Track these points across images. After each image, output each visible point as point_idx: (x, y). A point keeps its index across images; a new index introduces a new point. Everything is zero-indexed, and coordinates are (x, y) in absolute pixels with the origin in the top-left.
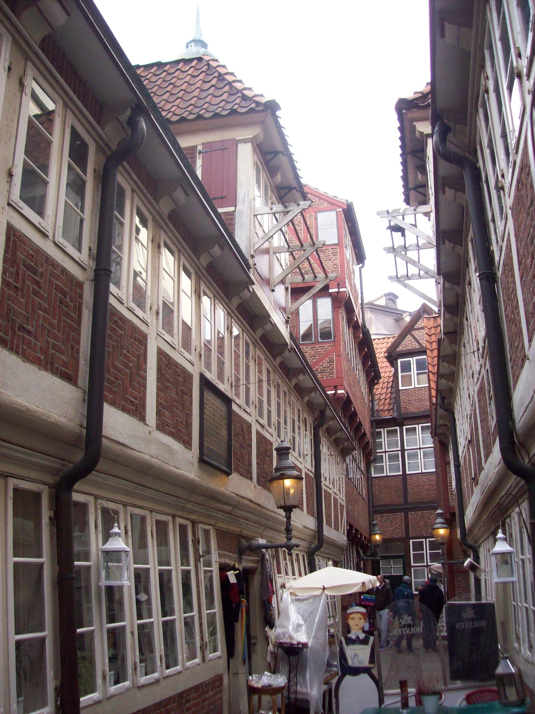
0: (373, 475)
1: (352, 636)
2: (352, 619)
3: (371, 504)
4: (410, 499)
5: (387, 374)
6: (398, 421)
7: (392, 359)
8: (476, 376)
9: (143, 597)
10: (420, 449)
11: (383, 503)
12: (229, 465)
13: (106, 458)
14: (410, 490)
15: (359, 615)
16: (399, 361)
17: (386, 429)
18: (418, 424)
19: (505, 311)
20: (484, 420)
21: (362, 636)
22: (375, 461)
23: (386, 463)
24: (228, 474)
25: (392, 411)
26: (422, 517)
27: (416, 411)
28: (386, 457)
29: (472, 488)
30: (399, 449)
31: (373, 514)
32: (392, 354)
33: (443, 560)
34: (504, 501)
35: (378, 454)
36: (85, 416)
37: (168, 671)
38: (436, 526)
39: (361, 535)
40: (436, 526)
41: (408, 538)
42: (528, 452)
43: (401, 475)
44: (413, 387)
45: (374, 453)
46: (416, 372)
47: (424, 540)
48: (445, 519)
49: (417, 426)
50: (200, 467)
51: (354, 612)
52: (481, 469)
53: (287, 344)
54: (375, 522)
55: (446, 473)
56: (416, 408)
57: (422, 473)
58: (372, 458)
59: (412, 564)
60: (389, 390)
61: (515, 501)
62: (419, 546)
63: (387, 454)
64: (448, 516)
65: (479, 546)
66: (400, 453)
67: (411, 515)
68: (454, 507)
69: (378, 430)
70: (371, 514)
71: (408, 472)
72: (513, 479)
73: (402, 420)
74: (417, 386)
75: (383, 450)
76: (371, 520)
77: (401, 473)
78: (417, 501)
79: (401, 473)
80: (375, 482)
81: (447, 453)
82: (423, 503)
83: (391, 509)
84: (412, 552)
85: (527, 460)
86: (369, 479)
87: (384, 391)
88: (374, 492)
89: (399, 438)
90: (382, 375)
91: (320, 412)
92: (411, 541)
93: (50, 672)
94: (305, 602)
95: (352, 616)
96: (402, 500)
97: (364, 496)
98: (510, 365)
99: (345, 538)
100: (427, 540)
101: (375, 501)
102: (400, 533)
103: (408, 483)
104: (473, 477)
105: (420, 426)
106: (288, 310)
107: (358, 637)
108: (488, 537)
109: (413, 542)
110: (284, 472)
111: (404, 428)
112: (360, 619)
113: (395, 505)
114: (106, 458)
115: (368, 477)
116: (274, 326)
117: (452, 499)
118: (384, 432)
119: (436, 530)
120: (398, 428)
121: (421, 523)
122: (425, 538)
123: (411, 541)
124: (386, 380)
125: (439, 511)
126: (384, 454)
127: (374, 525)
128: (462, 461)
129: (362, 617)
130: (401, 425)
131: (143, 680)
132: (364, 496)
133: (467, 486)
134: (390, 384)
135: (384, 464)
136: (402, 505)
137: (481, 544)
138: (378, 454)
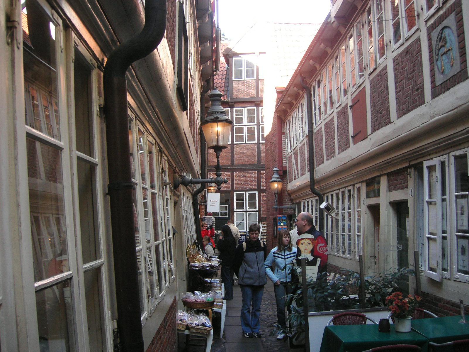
2: (302, 244)
4: (236, 162)
6: (230, 104)
7: (228, 57)
9: (349, 223)
10: (245, 125)
14: (236, 156)
15: (308, 241)
16: (234, 59)
18: (245, 107)
21: (311, 258)
25: (226, 96)
26: (244, 176)
32: (229, 53)
36: (444, 80)
38: (272, 180)
40: (272, 180)
41: (233, 190)
43: (230, 144)
46: (243, 69)
47: (245, 192)
49: (243, 108)
51: (304, 238)
56: (244, 95)
57: (245, 144)
59: (235, 210)
62: (240, 198)
63: (246, 127)
67: (236, 174)
68: (286, 167)
71: (235, 143)
73: (233, 103)
74: (246, 79)
75: (244, 124)
77: (256, 142)
78: (241, 164)
79: (256, 142)
87: (220, 81)
88: (209, 156)
92: (235, 193)
93: (108, 311)
96: (230, 162)
100: (247, 192)
103: (235, 150)
105: (246, 108)
109: (236, 194)
111: (234, 109)
112: (309, 244)
117: (285, 161)
119: (272, 184)
120: (229, 109)
121: (244, 180)
122: (246, 191)
123: (235, 193)
126: (244, 127)
129: (311, 242)
130: (232, 107)
134: (224, 76)
136: (229, 166)
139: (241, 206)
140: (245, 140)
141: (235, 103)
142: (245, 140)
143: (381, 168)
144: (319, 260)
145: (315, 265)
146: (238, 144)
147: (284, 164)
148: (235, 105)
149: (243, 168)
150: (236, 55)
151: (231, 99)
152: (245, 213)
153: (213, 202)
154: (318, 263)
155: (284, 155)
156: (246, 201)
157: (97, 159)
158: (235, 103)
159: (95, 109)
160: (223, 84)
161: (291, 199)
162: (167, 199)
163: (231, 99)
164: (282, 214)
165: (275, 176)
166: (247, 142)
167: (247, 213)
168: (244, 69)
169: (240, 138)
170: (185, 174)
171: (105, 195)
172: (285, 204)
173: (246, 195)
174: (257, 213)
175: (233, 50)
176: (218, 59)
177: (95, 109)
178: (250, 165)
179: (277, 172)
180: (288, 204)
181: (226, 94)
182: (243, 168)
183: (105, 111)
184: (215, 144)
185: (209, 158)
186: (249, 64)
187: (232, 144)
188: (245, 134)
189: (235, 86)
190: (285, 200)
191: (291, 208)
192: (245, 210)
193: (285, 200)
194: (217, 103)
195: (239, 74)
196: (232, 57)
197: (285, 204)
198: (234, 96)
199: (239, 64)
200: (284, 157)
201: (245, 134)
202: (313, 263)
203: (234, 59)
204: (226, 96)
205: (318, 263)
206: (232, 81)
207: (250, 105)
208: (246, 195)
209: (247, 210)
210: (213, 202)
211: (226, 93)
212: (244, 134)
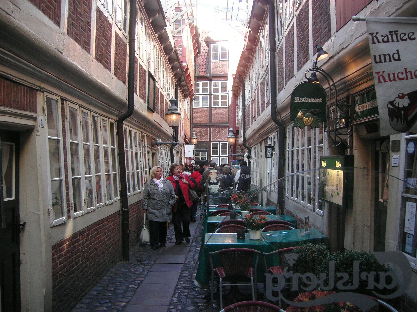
0: (193, 107)
1: (211, 181)
3: (191, 123)
4: (213, 121)
5: (204, 51)
8: (260, 77)
11: (198, 122)
12: (155, 110)
13: (361, 168)
15: (215, 173)
17: (202, 82)
19: (278, 65)
20: (263, 96)
21: (215, 181)
22: (195, 99)
23: (201, 100)
24: (154, 112)
25: (206, 72)
26: (219, 131)
27: (219, 73)
28: (201, 97)
29: (252, 122)
30: (209, 93)
31: (192, 128)
33: (231, 153)
34: (268, 130)
35: (197, 96)
37: (98, 205)
39: (187, 139)
41: (210, 141)
42: (280, 115)
43: (209, 108)
44: (219, 60)
45: (195, 95)
47: (219, 143)
48: (234, 133)
50: (148, 110)
52: (259, 115)
53: (172, 49)
54: (194, 132)
55: (236, 110)
57: (220, 107)
58: (193, 98)
59: (212, 155)
60: (205, 60)
61: (272, 130)
62: (216, 147)
64: (235, 132)
65: (251, 148)
66: (209, 95)
67: (212, 129)
69: (197, 82)
70: (191, 128)
71: (212, 106)
72: (273, 123)
75: (219, 93)
76: (191, 131)
77: (209, 107)
78: (217, 122)
80: (194, 110)
81: (237, 100)
82: (220, 123)
83: (203, 126)
84: (212, 149)
85: (280, 118)
86: (191, 109)
89: (209, 88)
90: (202, 51)
91: (179, 78)
92: (212, 143)
94: (89, 183)
95: (211, 173)
96: (208, 121)
97: (189, 118)
98: (277, 85)
99: (183, 140)
100: (221, 143)
101: (194, 121)
102: (206, 139)
104: (253, 117)
105: (221, 81)
106: (174, 32)
107: (214, 182)
108: (257, 144)
109: (213, 144)
110: (173, 111)
111: (212, 82)
113: (205, 123)
114: (361, 168)
115: (191, 108)
116: (170, 42)
117: (238, 123)
118: (201, 83)
120: (209, 82)
121: (218, 134)
122: (220, 142)
123: (212, 143)
124: (204, 54)
125: (231, 129)
126: (200, 96)
127: (193, 134)
128: (247, 107)
130: (210, 80)
131: (108, 202)
132: (189, 118)
133: (249, 120)
135: (200, 101)
136: (207, 123)
137: (253, 146)
138: (197, 96)
139: (216, 152)
140: (220, 105)
141: (213, 77)
142: (220, 105)
143: (262, 137)
144: (220, 182)
145: (217, 184)
146: (214, 108)
147: (237, 126)
148: (213, 79)
149: (219, 125)
150: (214, 42)
151: (210, 74)
152: (219, 157)
153: (189, 152)
154: (219, 184)
155: (237, 119)
156: (220, 149)
157: (115, 147)
158: (213, 77)
159: (115, 133)
160: (205, 63)
161: (241, 150)
162: (145, 153)
163: (210, 74)
164: (236, 159)
165: (231, 134)
166: (221, 106)
167: (220, 158)
168: (220, 53)
169: (215, 104)
170: (157, 139)
171: (118, 155)
172: (238, 153)
173: (220, 144)
174: (228, 158)
175: (211, 38)
176: (199, 45)
177: (115, 133)
178: (222, 123)
179: (232, 131)
180: (240, 153)
181: (207, 71)
182: (219, 125)
183: (118, 133)
184: (172, 125)
185: (193, 118)
186: (223, 49)
187: (210, 108)
188: (220, 100)
189: (212, 65)
190: (238, 150)
191: (241, 155)
192: (219, 156)
193: (238, 150)
194: (174, 104)
195: (216, 57)
196: (211, 44)
197: (238, 153)
198: (212, 73)
199: (216, 49)
200: (237, 121)
201: (220, 100)
202: (216, 184)
203: (212, 45)
204: (206, 72)
205: (219, 184)
206: (211, 61)
207: (224, 79)
208: (220, 144)
209: (221, 155)
210: (189, 152)
211: (206, 70)
212: (219, 101)
